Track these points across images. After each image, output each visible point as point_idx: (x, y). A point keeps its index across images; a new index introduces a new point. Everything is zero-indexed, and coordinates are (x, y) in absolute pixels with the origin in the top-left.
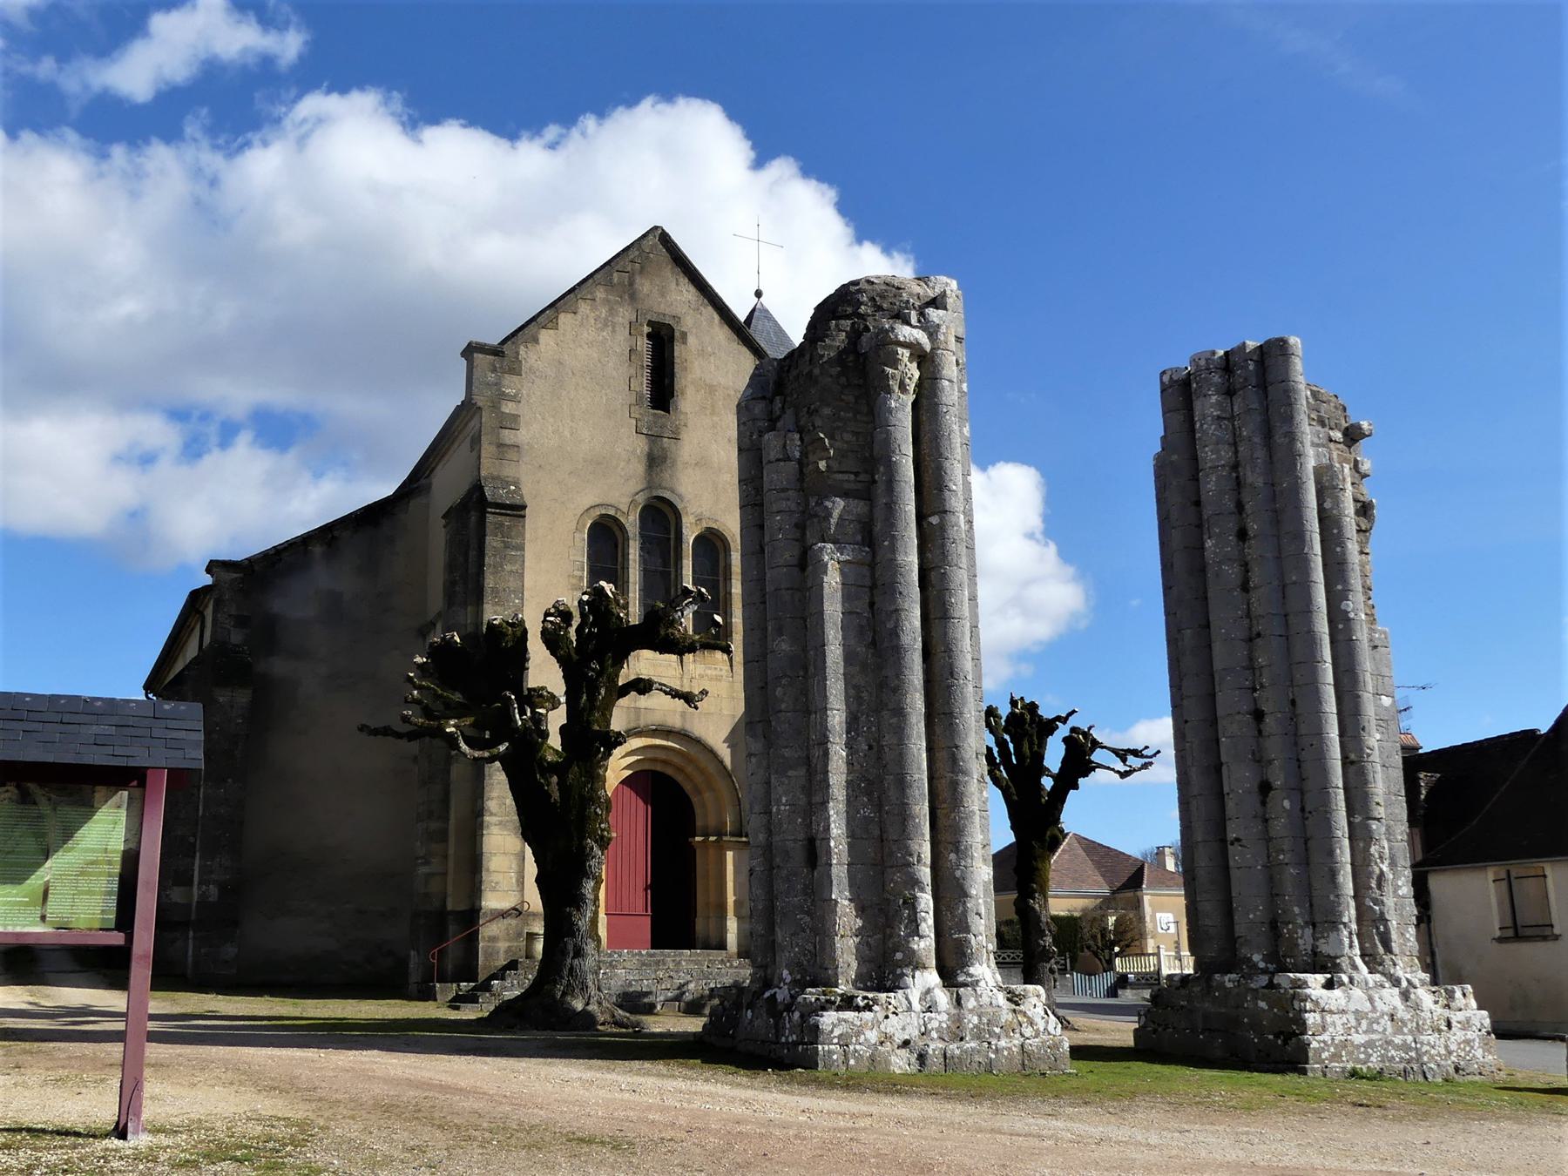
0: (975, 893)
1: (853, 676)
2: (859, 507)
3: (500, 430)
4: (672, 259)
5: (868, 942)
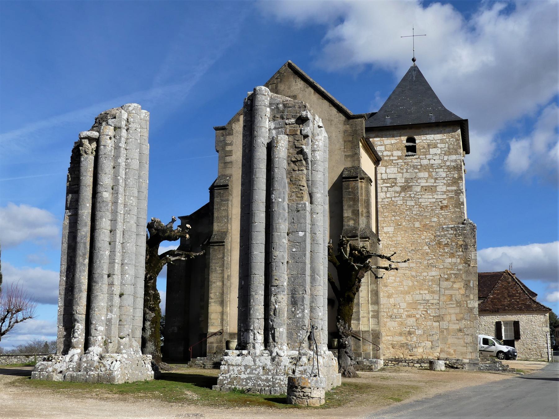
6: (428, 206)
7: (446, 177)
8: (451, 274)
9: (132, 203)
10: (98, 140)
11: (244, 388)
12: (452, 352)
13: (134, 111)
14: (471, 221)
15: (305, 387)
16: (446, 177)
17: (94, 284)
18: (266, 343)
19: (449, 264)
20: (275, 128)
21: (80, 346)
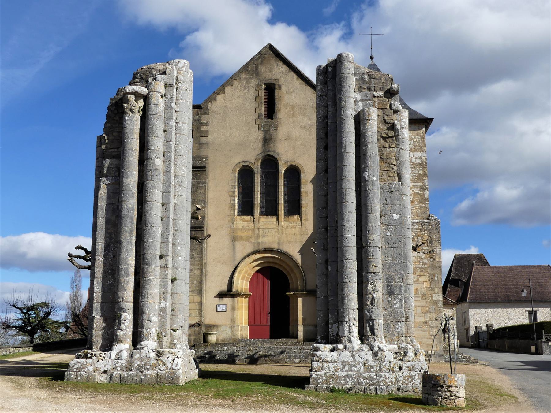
0: (148, 312)
1: (109, 229)
2: (115, 162)
3: (200, 138)
4: (275, 55)
5: (107, 333)
7: (412, 173)
8: (416, 268)
9: (184, 174)
10: (146, 98)
11: (344, 387)
13: (184, 69)
14: (436, 217)
15: (451, 386)
16: (412, 173)
17: (146, 266)
18: (362, 337)
20: (362, 100)
21: (128, 340)
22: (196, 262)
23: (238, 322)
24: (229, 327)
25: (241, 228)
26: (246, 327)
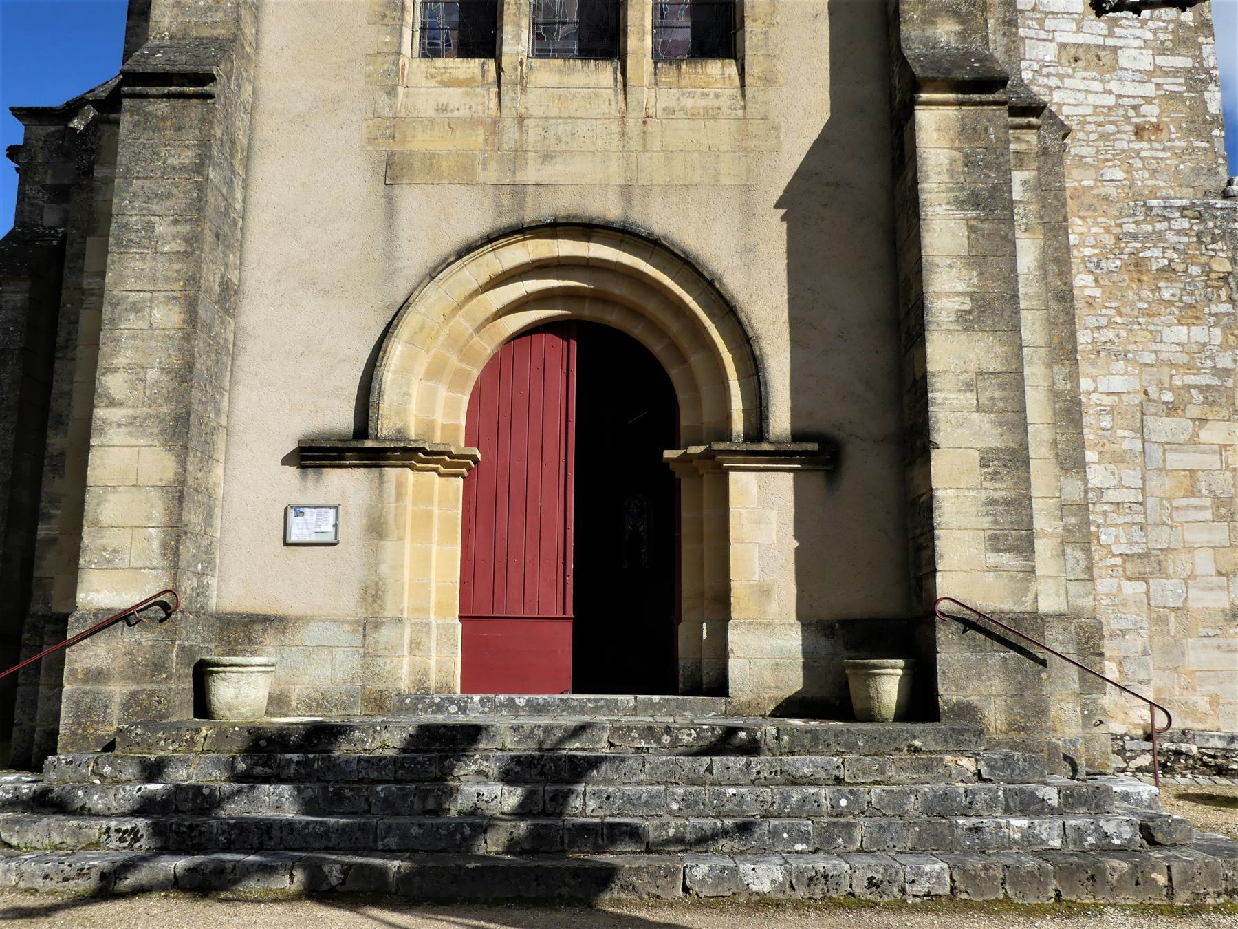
6: (1088, 119)
8: (1188, 388)
12: (1203, 704)
19: (1179, 349)
22: (161, 265)
23: (401, 601)
24: (346, 627)
25: (431, 113)
26: (445, 629)
